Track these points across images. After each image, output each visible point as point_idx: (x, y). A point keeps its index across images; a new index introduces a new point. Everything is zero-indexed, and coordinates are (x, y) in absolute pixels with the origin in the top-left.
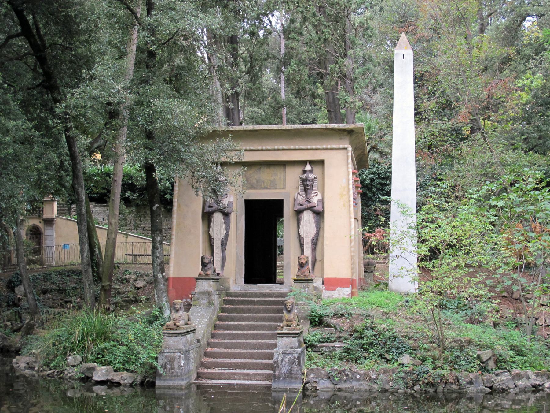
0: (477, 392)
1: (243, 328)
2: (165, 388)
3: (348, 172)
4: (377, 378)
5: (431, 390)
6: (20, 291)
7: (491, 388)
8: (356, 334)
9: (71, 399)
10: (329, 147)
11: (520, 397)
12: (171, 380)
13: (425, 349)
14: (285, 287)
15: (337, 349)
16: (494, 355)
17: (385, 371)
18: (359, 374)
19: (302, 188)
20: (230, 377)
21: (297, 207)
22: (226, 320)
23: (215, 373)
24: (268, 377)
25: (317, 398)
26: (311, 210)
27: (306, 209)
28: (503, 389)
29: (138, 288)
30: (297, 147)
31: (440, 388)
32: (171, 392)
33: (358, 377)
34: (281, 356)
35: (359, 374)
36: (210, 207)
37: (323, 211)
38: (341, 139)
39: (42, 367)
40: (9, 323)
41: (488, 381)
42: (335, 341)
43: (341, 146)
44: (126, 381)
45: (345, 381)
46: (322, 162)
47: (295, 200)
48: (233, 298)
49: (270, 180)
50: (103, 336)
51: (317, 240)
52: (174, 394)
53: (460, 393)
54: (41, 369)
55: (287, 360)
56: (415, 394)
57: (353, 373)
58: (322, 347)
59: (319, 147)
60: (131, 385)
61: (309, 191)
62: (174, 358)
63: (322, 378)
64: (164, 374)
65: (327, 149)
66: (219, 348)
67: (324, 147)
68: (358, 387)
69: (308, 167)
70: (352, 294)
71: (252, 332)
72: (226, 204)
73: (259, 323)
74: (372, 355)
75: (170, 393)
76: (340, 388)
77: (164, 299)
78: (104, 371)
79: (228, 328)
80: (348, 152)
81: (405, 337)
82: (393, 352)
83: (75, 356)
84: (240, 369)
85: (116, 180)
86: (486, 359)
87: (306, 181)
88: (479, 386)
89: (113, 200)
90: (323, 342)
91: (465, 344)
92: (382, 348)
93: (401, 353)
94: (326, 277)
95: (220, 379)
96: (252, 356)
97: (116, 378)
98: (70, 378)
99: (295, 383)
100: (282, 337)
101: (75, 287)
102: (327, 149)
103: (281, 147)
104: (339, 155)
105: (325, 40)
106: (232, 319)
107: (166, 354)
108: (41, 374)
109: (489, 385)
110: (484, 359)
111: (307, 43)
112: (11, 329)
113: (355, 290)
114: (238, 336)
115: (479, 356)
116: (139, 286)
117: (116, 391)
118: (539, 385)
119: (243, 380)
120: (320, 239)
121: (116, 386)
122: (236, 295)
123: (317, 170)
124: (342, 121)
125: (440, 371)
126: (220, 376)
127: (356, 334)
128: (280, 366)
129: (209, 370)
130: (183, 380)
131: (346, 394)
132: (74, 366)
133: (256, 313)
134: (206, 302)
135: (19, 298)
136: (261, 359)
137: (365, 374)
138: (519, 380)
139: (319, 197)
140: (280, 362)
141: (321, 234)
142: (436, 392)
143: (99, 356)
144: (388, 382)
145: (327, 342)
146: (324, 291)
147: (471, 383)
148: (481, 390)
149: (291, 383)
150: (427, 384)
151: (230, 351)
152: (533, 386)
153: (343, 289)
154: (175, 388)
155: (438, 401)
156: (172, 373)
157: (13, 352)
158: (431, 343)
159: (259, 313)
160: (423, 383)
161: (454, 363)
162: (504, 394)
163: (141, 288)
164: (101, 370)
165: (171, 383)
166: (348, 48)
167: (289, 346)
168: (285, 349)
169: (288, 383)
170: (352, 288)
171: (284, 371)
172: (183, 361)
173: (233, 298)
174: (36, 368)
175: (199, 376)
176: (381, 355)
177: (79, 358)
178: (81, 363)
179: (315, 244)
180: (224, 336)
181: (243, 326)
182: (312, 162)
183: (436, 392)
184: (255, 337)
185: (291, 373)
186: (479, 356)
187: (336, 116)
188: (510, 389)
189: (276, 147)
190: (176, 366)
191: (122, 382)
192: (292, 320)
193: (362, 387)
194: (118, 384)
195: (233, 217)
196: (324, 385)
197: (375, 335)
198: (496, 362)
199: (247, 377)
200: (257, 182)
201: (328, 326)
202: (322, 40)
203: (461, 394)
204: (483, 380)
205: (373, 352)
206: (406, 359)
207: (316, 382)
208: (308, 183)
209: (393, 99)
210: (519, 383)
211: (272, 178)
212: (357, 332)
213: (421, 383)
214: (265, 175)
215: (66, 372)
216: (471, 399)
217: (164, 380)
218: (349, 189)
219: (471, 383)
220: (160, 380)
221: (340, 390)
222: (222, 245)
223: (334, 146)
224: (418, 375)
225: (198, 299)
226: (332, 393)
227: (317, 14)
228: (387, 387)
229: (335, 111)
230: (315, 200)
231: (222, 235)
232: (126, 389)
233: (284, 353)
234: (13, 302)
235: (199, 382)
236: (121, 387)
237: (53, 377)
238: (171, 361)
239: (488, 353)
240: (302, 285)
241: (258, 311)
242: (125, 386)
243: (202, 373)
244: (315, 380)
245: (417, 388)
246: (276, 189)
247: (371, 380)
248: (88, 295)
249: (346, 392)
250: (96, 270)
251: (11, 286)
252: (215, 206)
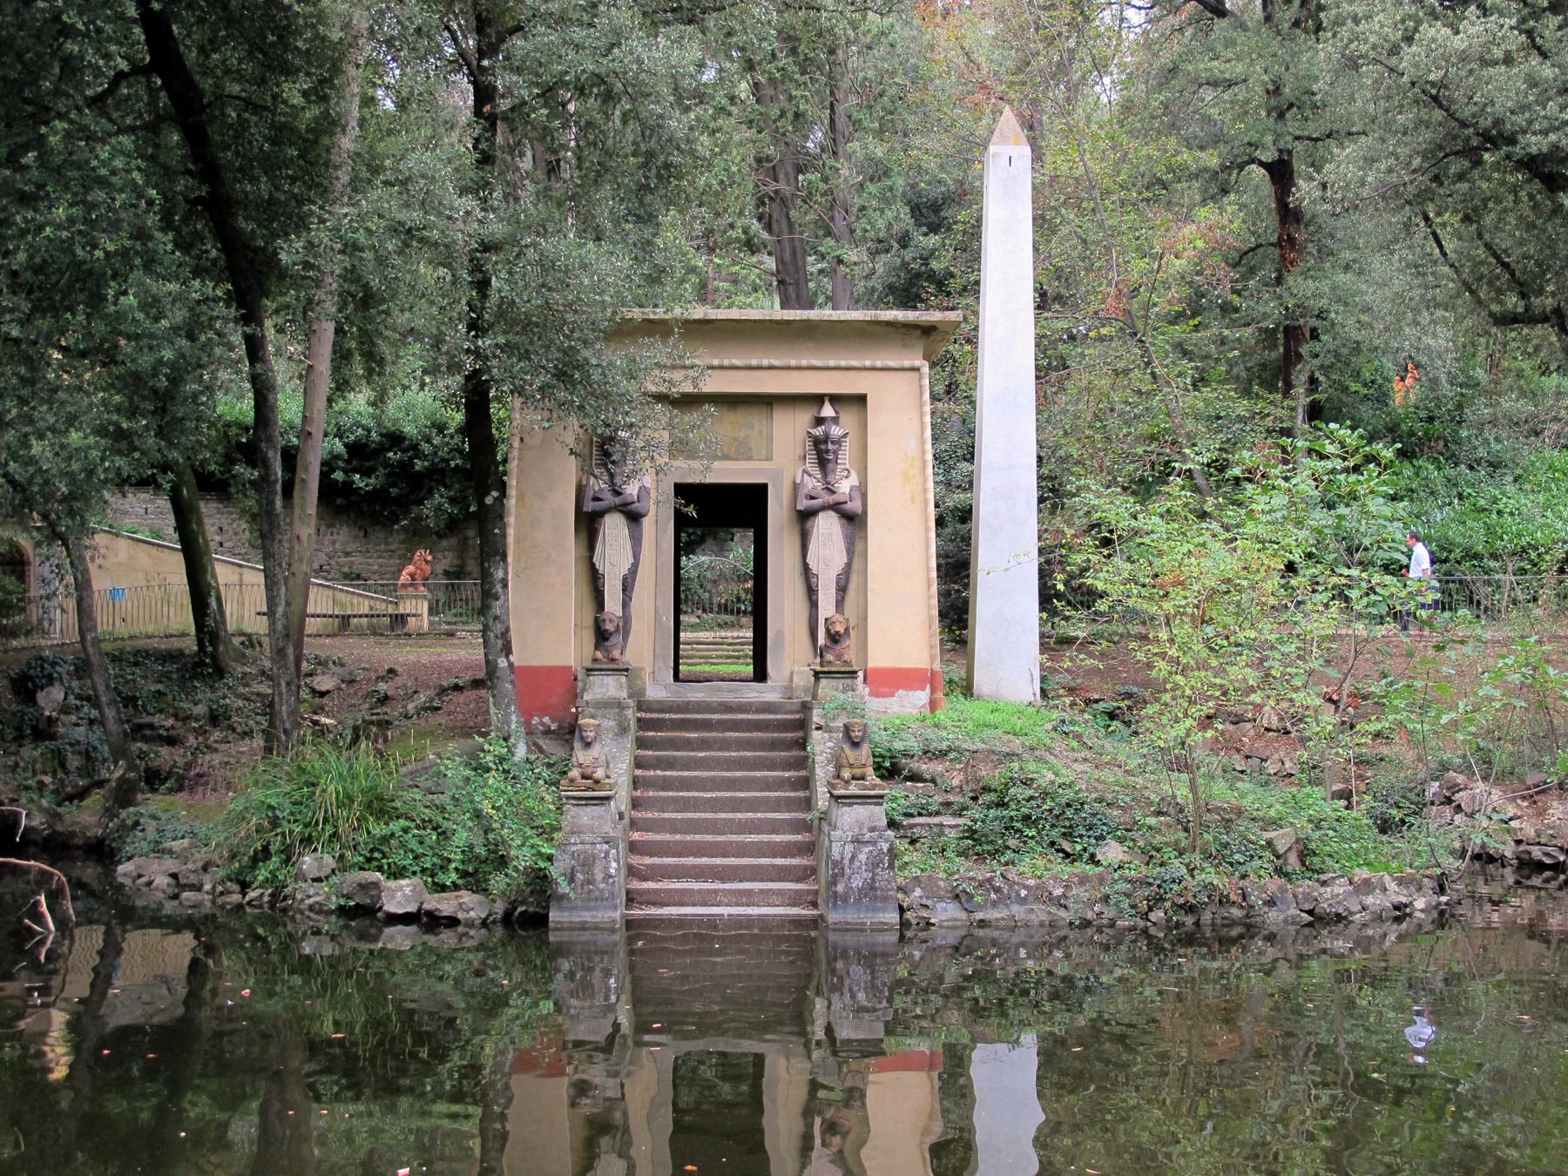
0: (1285, 921)
1: (702, 785)
2: (846, 929)
3: (922, 423)
4: (1064, 895)
5: (1189, 920)
6: (51, 698)
7: (1310, 912)
8: (992, 797)
9: (308, 959)
10: (879, 364)
11: (1370, 932)
12: (589, 909)
13: (1150, 828)
14: (773, 689)
15: (947, 831)
16: (1298, 841)
17: (1083, 880)
18: (1025, 887)
19: (812, 458)
20: (705, 899)
21: (803, 504)
22: (655, 767)
23: (669, 891)
24: (794, 899)
26: (837, 511)
27: (824, 508)
28: (1338, 915)
29: (322, 694)
30: (804, 363)
31: (1206, 917)
32: (586, 936)
33: (1023, 893)
34: (849, 848)
35: (1025, 887)
36: (596, 499)
37: (865, 512)
38: (905, 346)
39: (222, 882)
40: (47, 779)
41: (1307, 897)
42: (938, 813)
43: (907, 364)
44: (472, 914)
45: (994, 904)
46: (861, 400)
47: (796, 487)
48: (655, 715)
50: (379, 807)
51: (847, 580)
52: (595, 943)
53: (1248, 926)
54: (220, 888)
55: (863, 857)
56: (1153, 931)
57: (1011, 884)
58: (912, 826)
59: (854, 363)
60: (484, 923)
61: (830, 466)
62: (594, 857)
63: (941, 899)
64: (572, 895)
66: (658, 832)
67: (868, 363)
68: (1023, 916)
69: (828, 411)
70: (933, 705)
71: (728, 794)
72: (635, 493)
73: (738, 774)
74: (1032, 843)
78: (408, 890)
79: (666, 784)
80: (920, 379)
81: (1100, 800)
82: (1081, 836)
83: (319, 854)
84: (723, 880)
85: (310, 434)
87: (826, 442)
89: (303, 480)
90: (912, 815)
91: (1233, 816)
92: (1053, 826)
93: (1101, 838)
94: (870, 665)
95: (682, 905)
96: (742, 850)
97: (444, 905)
98: (311, 908)
99: (884, 910)
100: (851, 805)
101: (159, 692)
103: (765, 362)
104: (903, 383)
105: (797, 115)
106: (670, 764)
107: (574, 848)
108: (220, 901)
109: (1307, 907)
110: (1281, 850)
111: (751, 122)
112: (56, 792)
113: (940, 695)
114: (695, 805)
115: (1270, 843)
116: (323, 689)
117: (447, 938)
118: (1406, 906)
119: (737, 905)
120: (854, 579)
121: (447, 926)
122: (663, 707)
123: (848, 418)
124: (811, 305)
125: (1200, 877)
126: (681, 898)
127: (992, 797)
128: (848, 871)
129: (651, 885)
131: (996, 934)
132: (318, 880)
133: (720, 749)
134: (612, 723)
135: (50, 718)
136: (764, 856)
137: (1038, 887)
139: (854, 480)
140: (846, 862)
141: (856, 565)
142: (1197, 924)
143: (376, 855)
144: (1091, 903)
145: (920, 815)
146: (867, 698)
147: (1271, 903)
149: (875, 910)
150: (1181, 906)
151: (689, 838)
152: (1396, 908)
154: (596, 927)
155: (1200, 945)
156: (590, 891)
157: (78, 848)
158: (1159, 813)
159: (728, 750)
160: (1174, 904)
161: (1220, 856)
162: (1341, 926)
163: (328, 692)
164: (401, 888)
165: (587, 916)
166: (840, 138)
168: (857, 831)
169: (867, 910)
170: (933, 692)
171: (857, 882)
173: (655, 715)
174: (207, 887)
175: (631, 899)
176: (1052, 844)
177: (329, 861)
178: (333, 871)
179: (842, 589)
180: (664, 805)
181: (702, 779)
182: (835, 399)
183: (1197, 924)
184: (736, 805)
185: (873, 888)
186: (1270, 843)
187: (798, 296)
188: (1351, 913)
189: (754, 362)
190: (599, 876)
191: (460, 916)
192: (864, 766)
193: (1033, 917)
194: (453, 922)
195: (647, 522)
196: (946, 913)
197: (1032, 798)
198: (1302, 857)
199: (748, 898)
201: (915, 777)
202: (790, 115)
203: (1250, 929)
204: (1295, 896)
205: (1033, 837)
206: (1112, 852)
207: (926, 906)
208: (830, 446)
210: (1369, 900)
211: (742, 435)
212: (990, 790)
213: (1168, 904)
215: (299, 896)
216: (1271, 938)
217: (570, 909)
218: (924, 462)
219: (1271, 903)
220: (561, 908)
221: (983, 924)
222: (624, 590)
224: (1159, 886)
226: (963, 932)
227: (779, 55)
228: (1090, 915)
229: (797, 283)
230: (845, 487)
231: (624, 570)
232: (472, 933)
233: (858, 841)
234: (34, 728)
236: (460, 929)
237: (261, 907)
238: (587, 863)
239: (1287, 834)
240: (841, 683)
241: (725, 745)
242: (470, 924)
243: (638, 891)
244: (924, 901)
245: (1157, 915)
246: (750, 459)
247: (1051, 899)
248: (284, 708)
249: (997, 928)
250: (210, 649)
251: (26, 686)
252: (609, 499)
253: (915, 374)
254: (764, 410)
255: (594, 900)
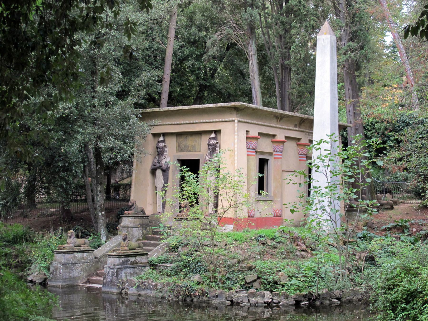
0: (219, 303)
10: (223, 120)
12: (55, 282)
15: (168, 268)
25: (129, 300)
30: (204, 121)
34: (108, 269)
35: (152, 285)
38: (231, 113)
43: (231, 119)
46: (218, 132)
49: (192, 145)
55: (110, 272)
58: (160, 266)
65: (222, 121)
67: (221, 120)
75: (54, 290)
76: (140, 294)
77: (102, 230)
86: (250, 281)
88: (222, 299)
99: (113, 288)
100: (110, 257)
102: (222, 121)
109: (229, 299)
130: (60, 282)
138: (253, 297)
148: (222, 302)
149: (111, 288)
152: (265, 303)
153: (229, 226)
167: (113, 263)
172: (61, 270)
182: (164, 135)
185: (112, 282)
189: (192, 122)
190: (58, 273)
196: (132, 291)
200: (185, 147)
203: (209, 305)
209: (338, 75)
211: (194, 144)
214: (190, 141)
223: (227, 120)
225: (122, 230)
235: (89, 285)
238: (56, 269)
244: (128, 287)
246: (196, 151)
253: (232, 123)
254: (185, 136)
255: (57, 279)
